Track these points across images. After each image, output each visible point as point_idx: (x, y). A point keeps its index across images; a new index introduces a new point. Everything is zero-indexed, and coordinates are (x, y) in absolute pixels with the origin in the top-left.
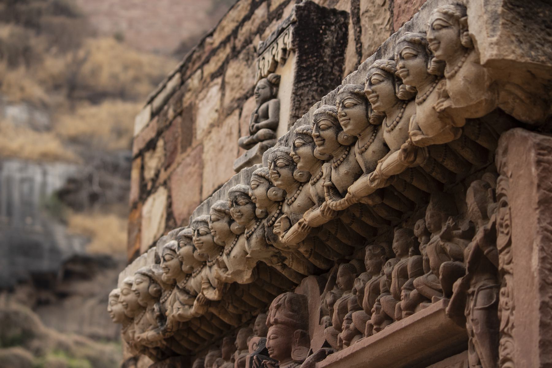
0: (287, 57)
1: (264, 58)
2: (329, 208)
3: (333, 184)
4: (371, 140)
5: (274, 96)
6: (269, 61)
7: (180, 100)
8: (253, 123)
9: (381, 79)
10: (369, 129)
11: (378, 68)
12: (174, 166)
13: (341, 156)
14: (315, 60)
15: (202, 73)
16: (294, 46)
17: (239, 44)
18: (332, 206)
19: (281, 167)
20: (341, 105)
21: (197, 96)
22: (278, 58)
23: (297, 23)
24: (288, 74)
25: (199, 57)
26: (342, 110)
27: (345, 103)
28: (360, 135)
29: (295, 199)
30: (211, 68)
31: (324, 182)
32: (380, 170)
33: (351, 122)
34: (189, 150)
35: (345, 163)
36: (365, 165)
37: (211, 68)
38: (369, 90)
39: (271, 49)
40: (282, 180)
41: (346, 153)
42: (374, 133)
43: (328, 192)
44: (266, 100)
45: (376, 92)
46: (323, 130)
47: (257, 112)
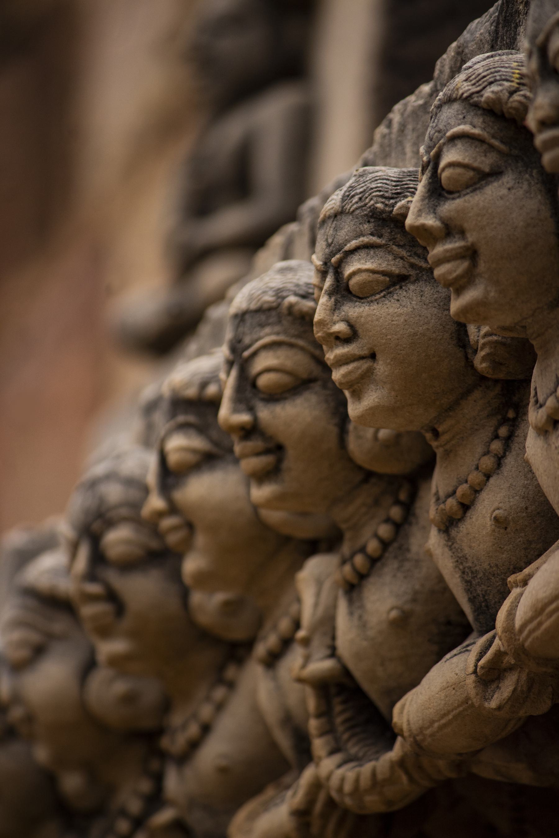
2: (331, 803)
3: (346, 672)
4: (487, 462)
9: (485, 162)
10: (475, 406)
11: (470, 103)
13: (374, 532)
18: (340, 789)
19: (128, 566)
20: (329, 281)
26: (336, 307)
27: (348, 270)
28: (436, 434)
29: (206, 729)
31: (307, 659)
32: (509, 629)
33: (381, 368)
35: (390, 567)
36: (469, 586)
38: (430, 221)
40: (133, 635)
41: (396, 512)
42: (504, 421)
43: (325, 713)
45: (462, 233)
46: (274, 396)
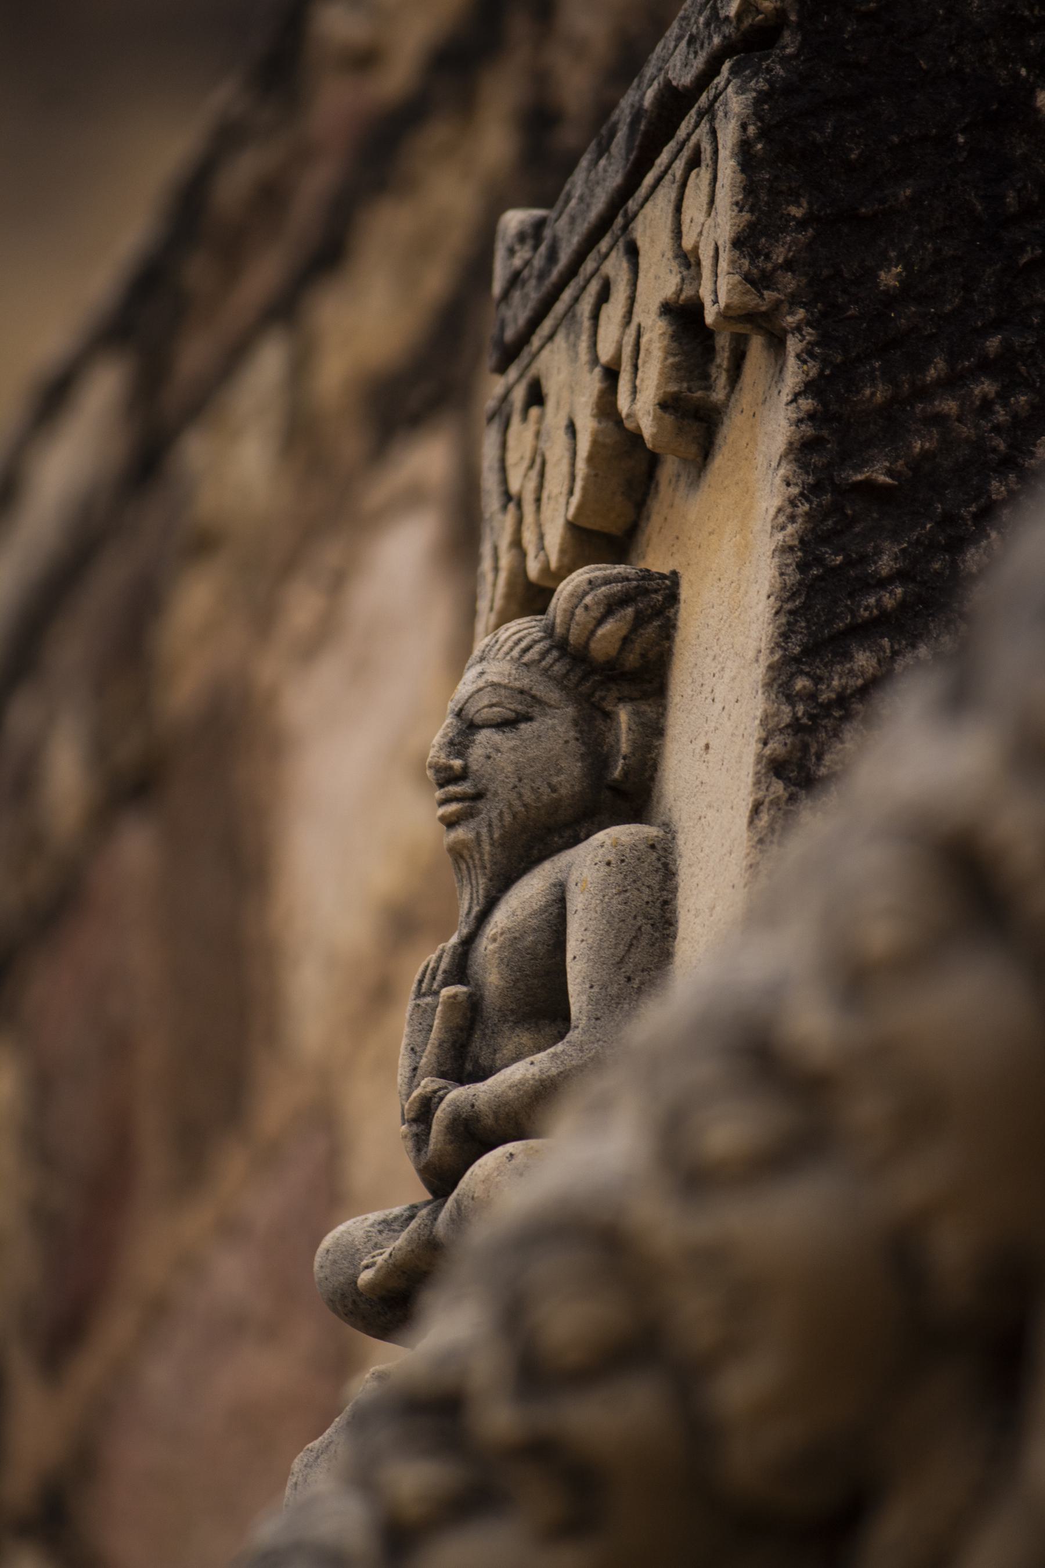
0: (718, 395)
1: (536, 396)
5: (626, 791)
6: (571, 429)
7: (132, 648)
8: (427, 1084)
12: (117, 1328)
14: (986, 406)
15: (300, 368)
16: (756, 281)
17: (575, 85)
21: (263, 618)
22: (642, 405)
23: (790, 43)
24: (731, 563)
25: (271, 196)
30: (368, 320)
34: (233, 1166)
37: (368, 320)
39: (585, 307)
44: (538, 836)
47: (460, 968)
